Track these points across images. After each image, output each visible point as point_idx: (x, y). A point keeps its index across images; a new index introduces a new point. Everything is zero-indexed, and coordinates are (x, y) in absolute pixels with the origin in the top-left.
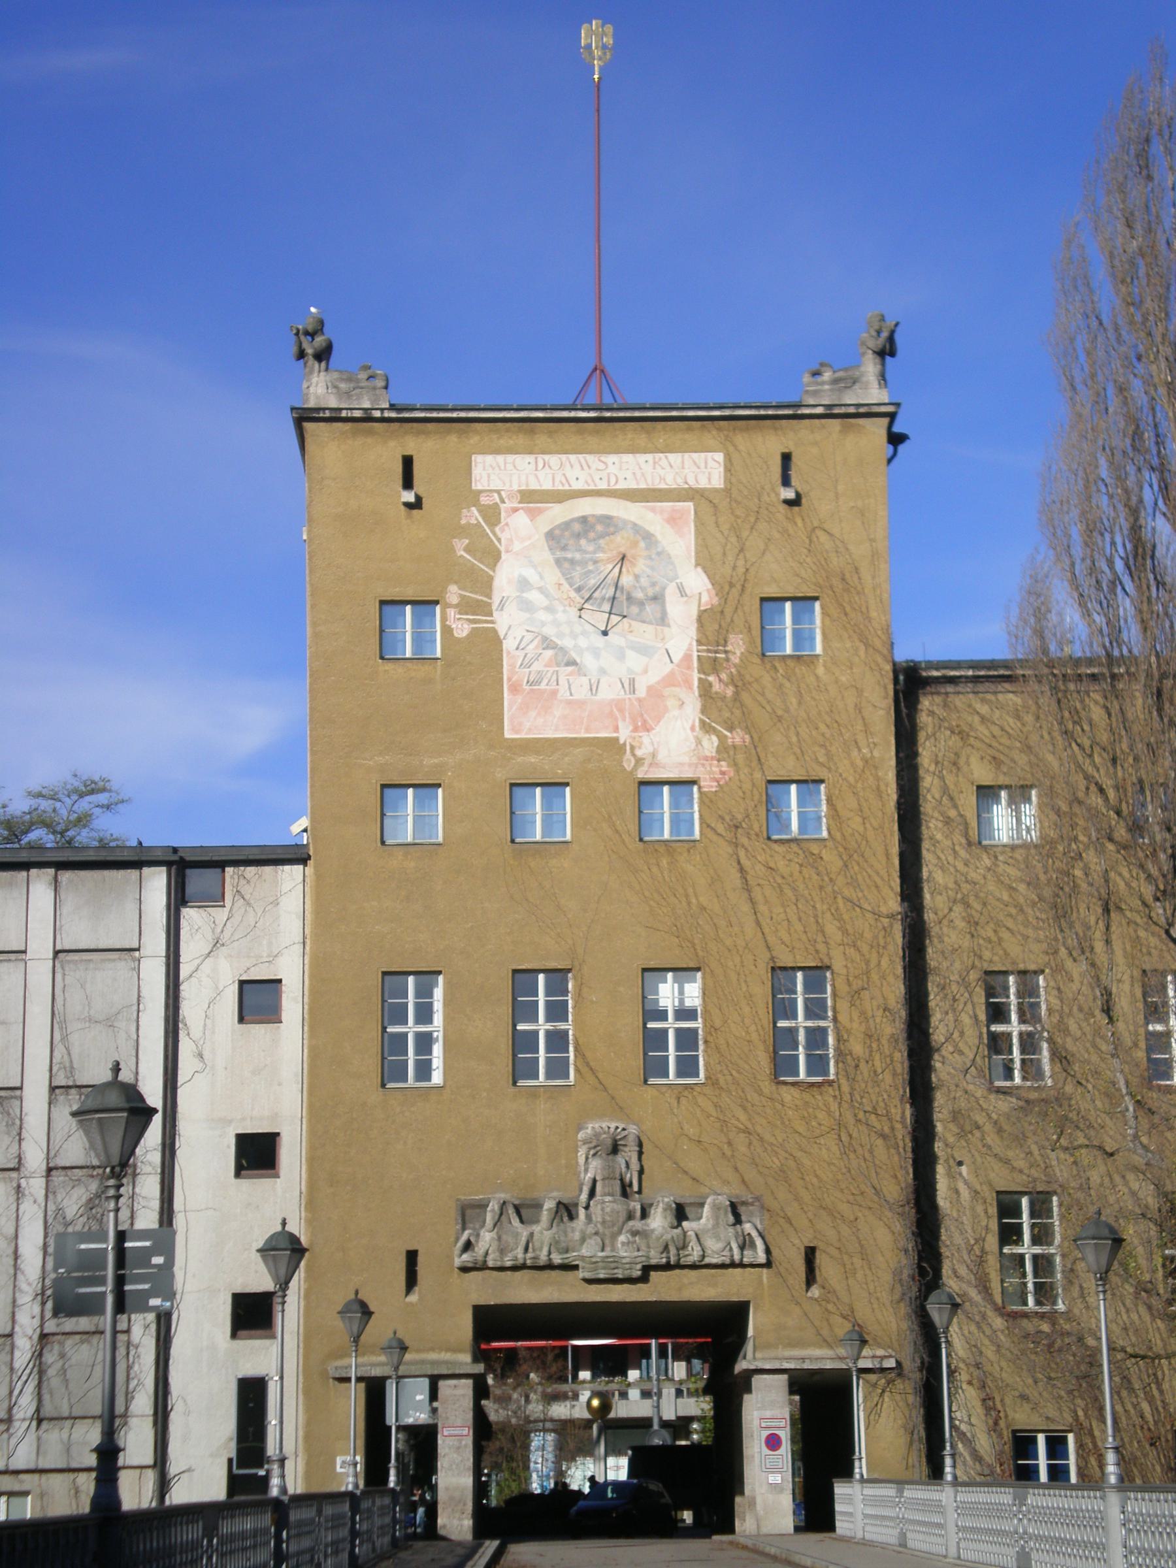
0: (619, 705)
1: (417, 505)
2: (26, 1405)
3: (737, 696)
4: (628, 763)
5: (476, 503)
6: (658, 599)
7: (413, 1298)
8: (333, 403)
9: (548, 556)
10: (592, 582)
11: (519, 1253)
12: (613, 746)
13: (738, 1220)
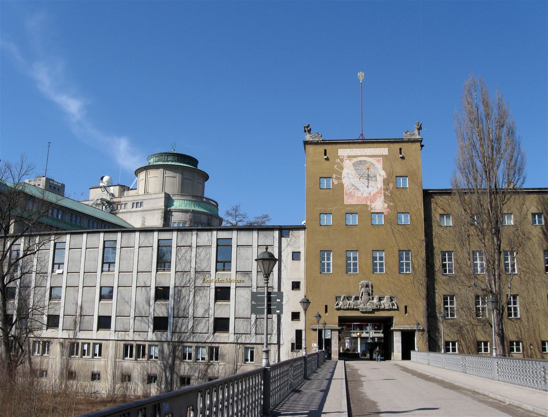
0: (367, 197)
1: (403, 158)
2: (253, 331)
3: (391, 196)
4: (369, 209)
5: (339, 158)
6: (375, 176)
7: (327, 314)
8: (311, 140)
9: (353, 168)
10: (362, 173)
11: (348, 306)
12: (366, 206)
13: (392, 300)
